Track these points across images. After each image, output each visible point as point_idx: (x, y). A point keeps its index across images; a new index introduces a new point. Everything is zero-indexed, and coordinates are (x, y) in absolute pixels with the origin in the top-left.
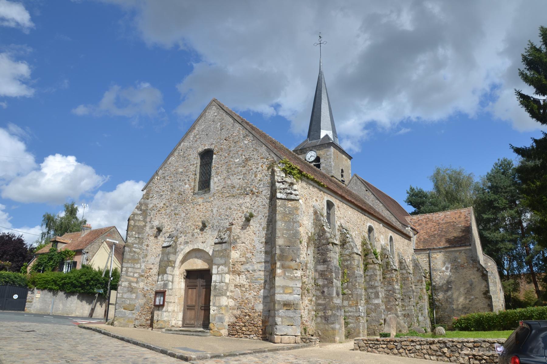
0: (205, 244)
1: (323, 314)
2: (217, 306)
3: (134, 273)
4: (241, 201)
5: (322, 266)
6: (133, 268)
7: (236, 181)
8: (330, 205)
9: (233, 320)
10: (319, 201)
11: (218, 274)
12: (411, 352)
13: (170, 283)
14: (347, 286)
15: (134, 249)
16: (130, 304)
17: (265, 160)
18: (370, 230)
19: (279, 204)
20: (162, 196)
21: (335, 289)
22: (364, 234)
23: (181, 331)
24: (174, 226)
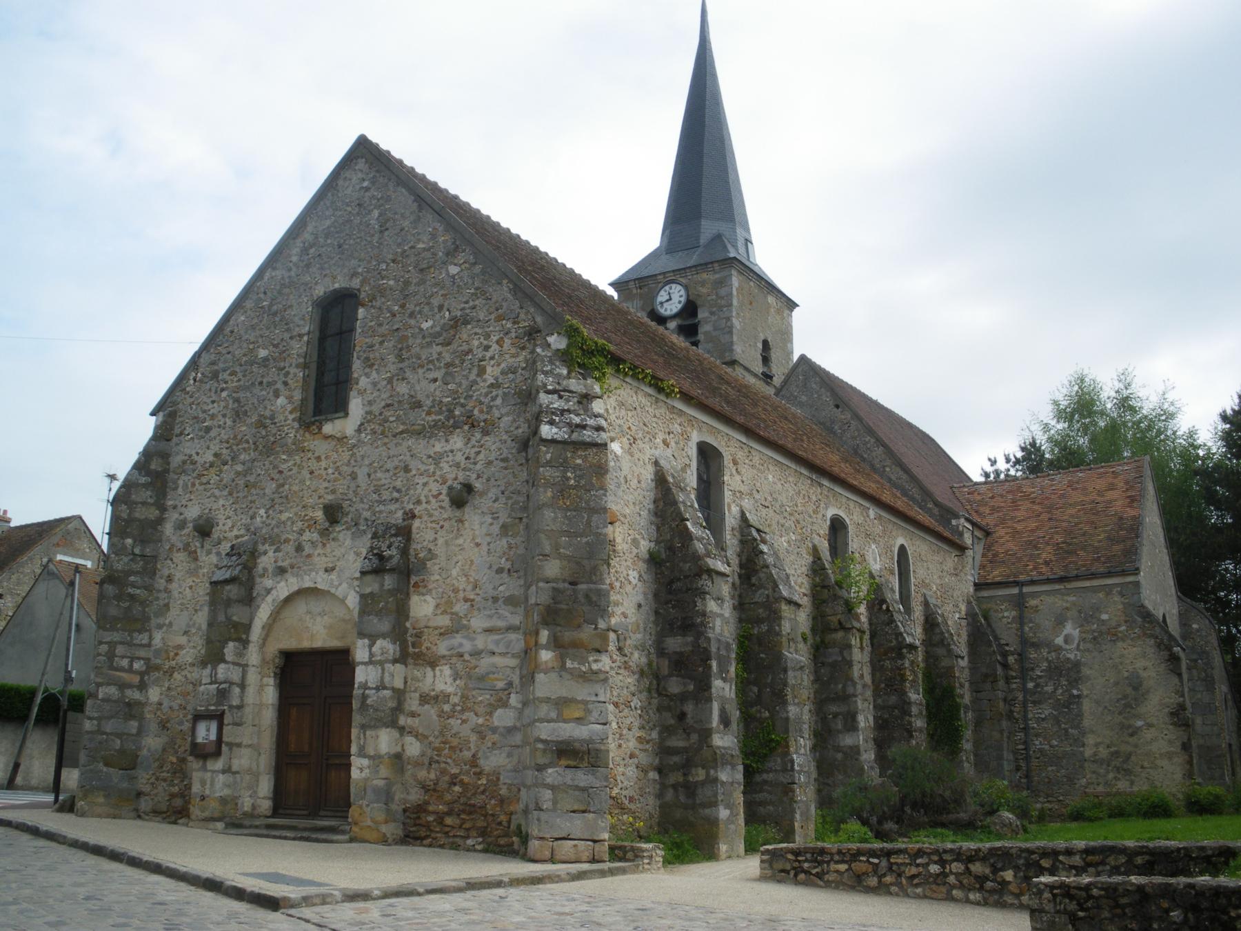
0: (334, 576)
1: (681, 779)
2: (370, 757)
3: (132, 659)
4: (439, 447)
5: (679, 639)
6: (130, 644)
7: (425, 385)
8: (707, 454)
9: (415, 796)
10: (673, 444)
11: (371, 662)
12: (916, 881)
13: (237, 690)
14: (759, 696)
15: (130, 590)
16: (122, 752)
17: (509, 325)
18: (837, 526)
19: (548, 456)
20: (208, 429)
21: (716, 707)
22: (817, 540)
23: (269, 827)
24: (246, 520)
